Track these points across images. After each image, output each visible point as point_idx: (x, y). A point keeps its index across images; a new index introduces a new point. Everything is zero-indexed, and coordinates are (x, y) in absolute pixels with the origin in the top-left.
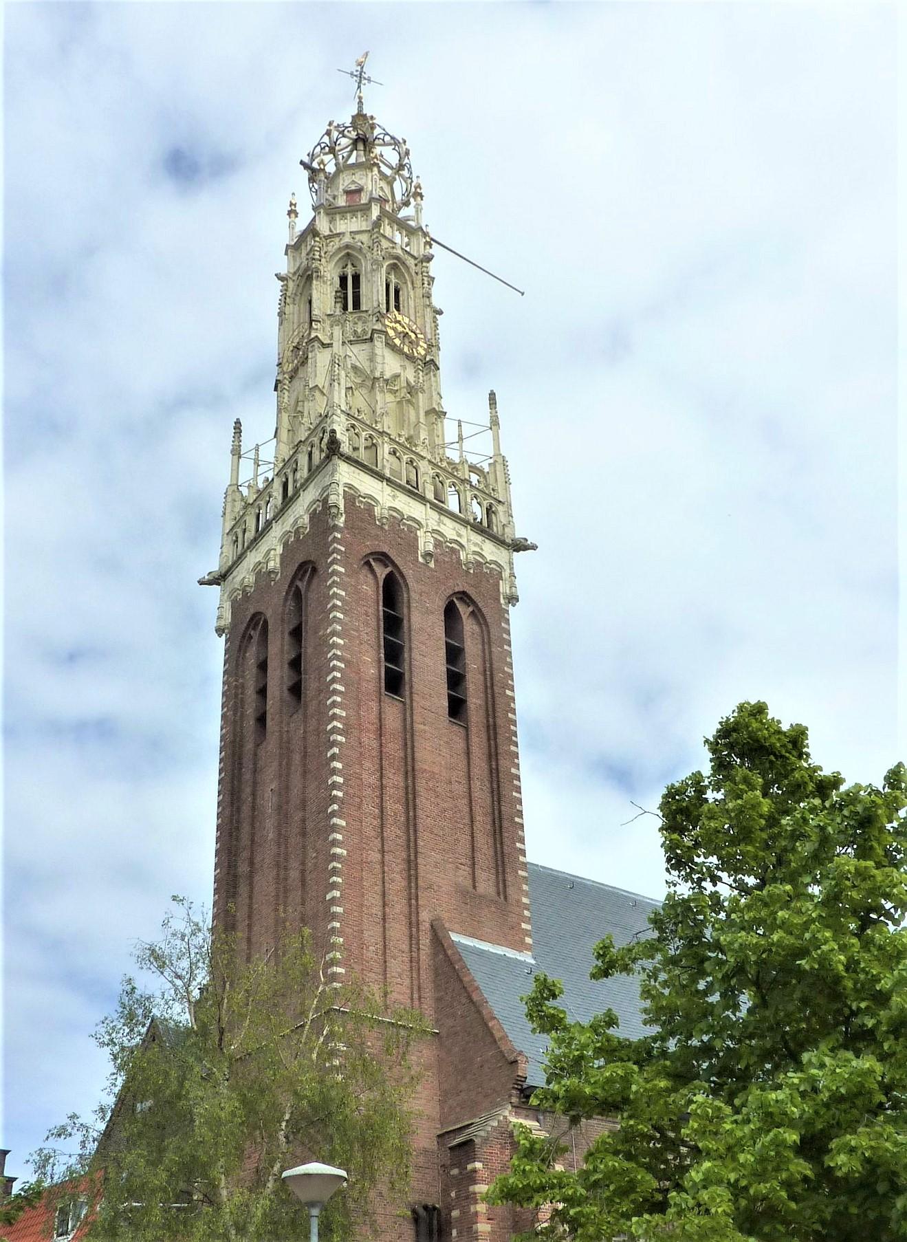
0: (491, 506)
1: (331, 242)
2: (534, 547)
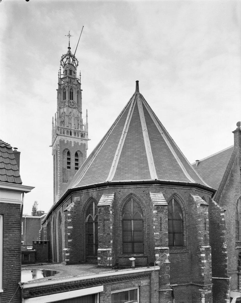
0: (71, 131)
2: (90, 140)
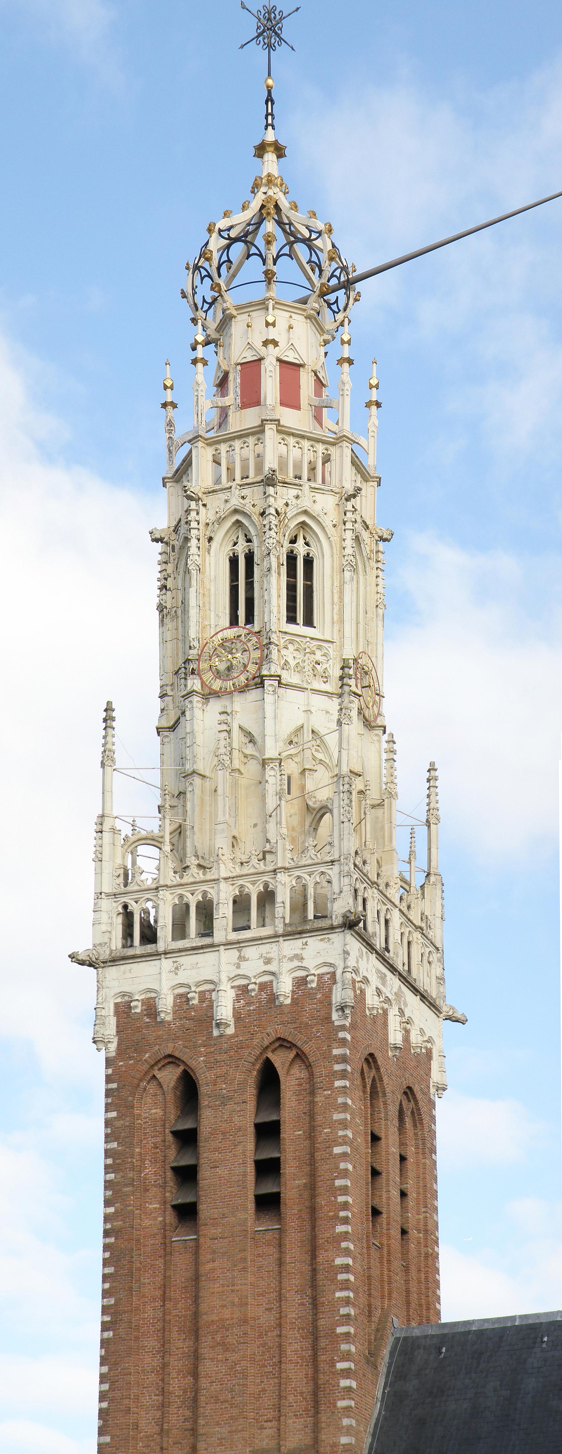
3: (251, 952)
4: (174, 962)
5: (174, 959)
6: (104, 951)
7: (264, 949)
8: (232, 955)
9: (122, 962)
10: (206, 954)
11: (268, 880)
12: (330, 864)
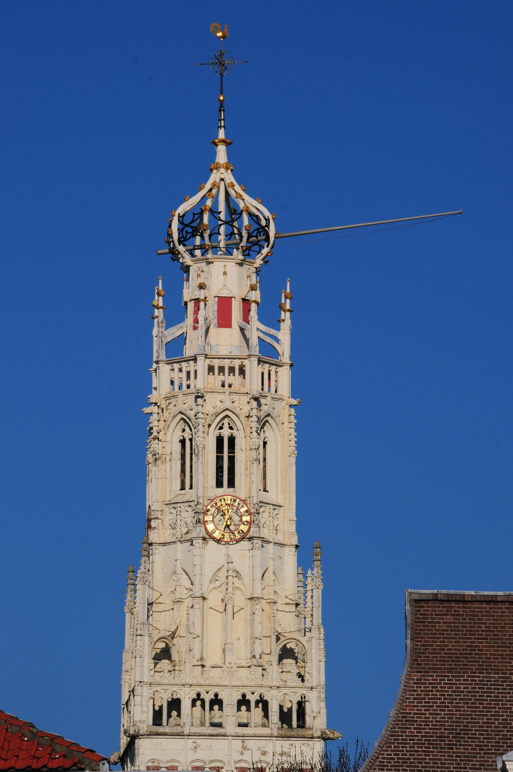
1: (169, 403)
3: (251, 744)
4: (194, 742)
5: (194, 740)
6: (143, 727)
7: (262, 743)
8: (237, 744)
9: (155, 737)
10: (246, 760)
11: (264, 692)
12: (310, 689)
